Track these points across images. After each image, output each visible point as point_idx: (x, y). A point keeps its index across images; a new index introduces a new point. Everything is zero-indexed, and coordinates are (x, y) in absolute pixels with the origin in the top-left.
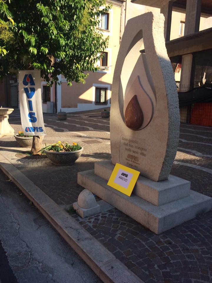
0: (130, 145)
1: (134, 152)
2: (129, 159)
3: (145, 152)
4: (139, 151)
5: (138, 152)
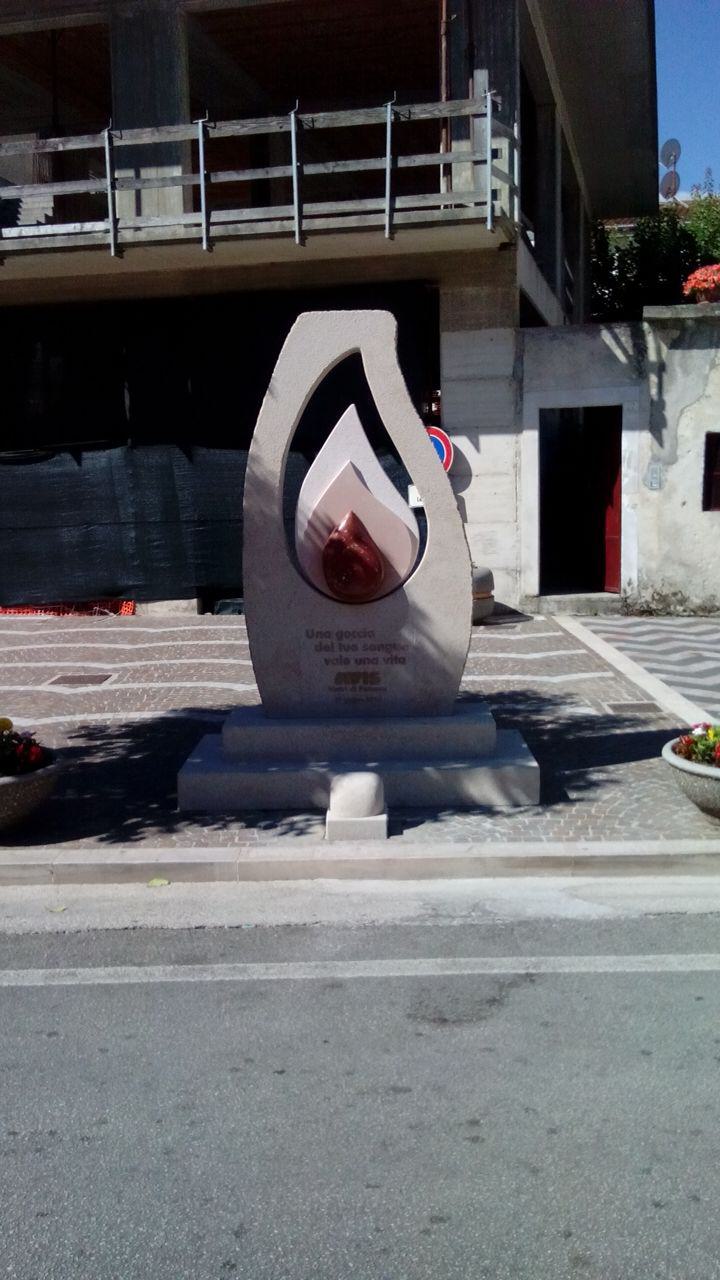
1: (360, 662)
2: (343, 686)
4: (381, 655)
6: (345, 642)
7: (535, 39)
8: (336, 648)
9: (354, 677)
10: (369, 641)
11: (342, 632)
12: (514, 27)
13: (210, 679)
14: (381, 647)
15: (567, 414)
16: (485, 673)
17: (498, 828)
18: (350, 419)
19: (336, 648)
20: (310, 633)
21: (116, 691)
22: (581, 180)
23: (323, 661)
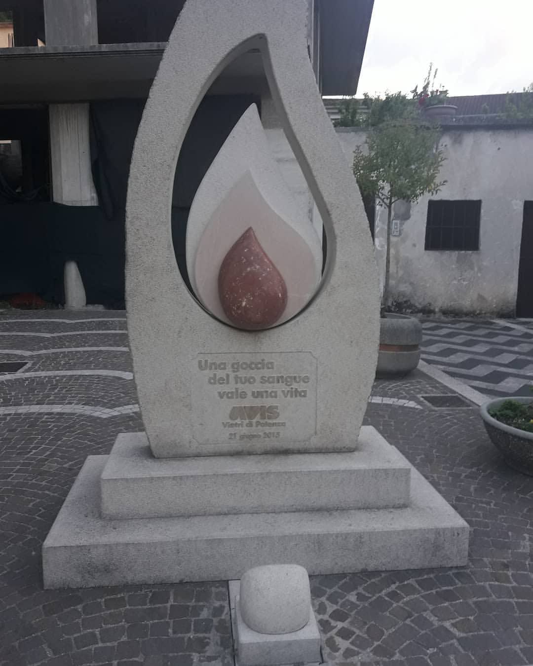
0: (236, 377)
1: (258, 395)
2: (238, 421)
3: (301, 386)
4: (280, 388)
5: (276, 392)
6: (242, 374)
9: (251, 412)
10: (266, 373)
13: (105, 367)
14: (279, 379)
15: (122, 309)
20: (203, 363)
21: (27, 379)
23: (217, 395)
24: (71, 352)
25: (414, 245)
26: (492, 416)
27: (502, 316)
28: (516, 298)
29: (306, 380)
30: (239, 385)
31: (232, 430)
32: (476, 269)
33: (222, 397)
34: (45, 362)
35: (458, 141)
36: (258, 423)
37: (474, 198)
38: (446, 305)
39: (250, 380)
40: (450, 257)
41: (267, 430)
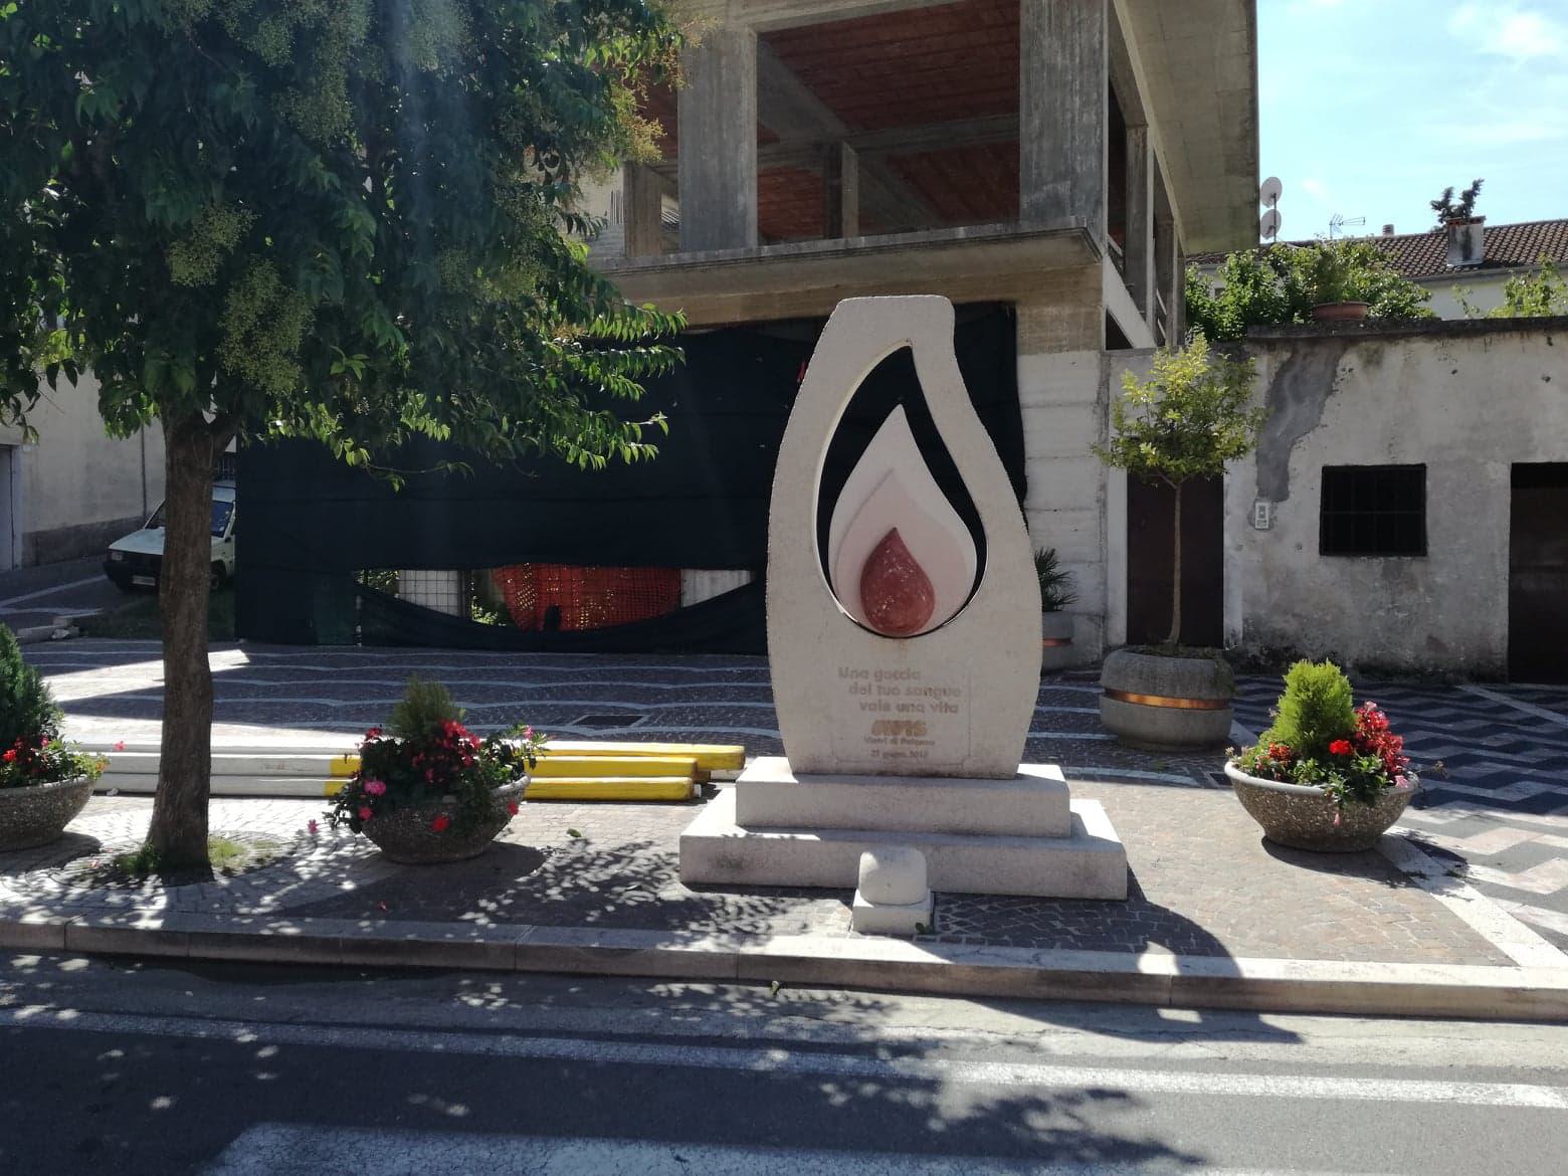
1: (903, 708)
2: (882, 737)
3: (952, 700)
5: (923, 707)
6: (885, 683)
7: (1125, 51)
8: (874, 690)
9: (896, 727)
10: (913, 683)
11: (881, 672)
12: (1101, 33)
13: (749, 724)
14: (928, 691)
16: (1061, 730)
17: (1071, 929)
18: (897, 421)
19: (874, 690)
22: (1175, 212)
24: (703, 707)
25: (1299, 547)
26: (1254, 774)
27: (1479, 676)
28: (1506, 644)
29: (956, 692)
30: (883, 697)
31: (875, 747)
32: (1422, 590)
33: (863, 708)
34: (667, 716)
35: (1373, 361)
36: (903, 740)
37: (1410, 459)
38: (1365, 657)
39: (894, 691)
40: (1368, 570)
41: (914, 748)
